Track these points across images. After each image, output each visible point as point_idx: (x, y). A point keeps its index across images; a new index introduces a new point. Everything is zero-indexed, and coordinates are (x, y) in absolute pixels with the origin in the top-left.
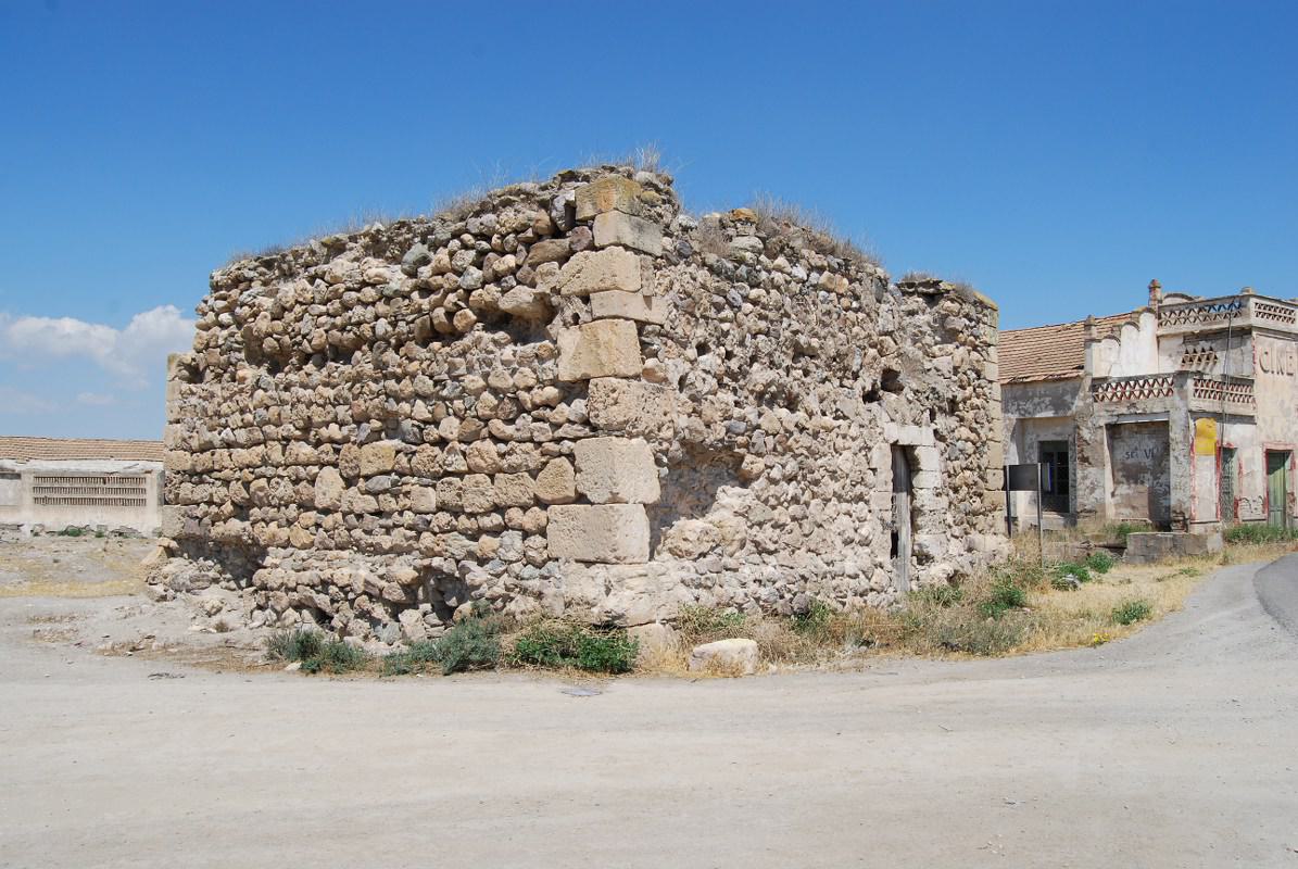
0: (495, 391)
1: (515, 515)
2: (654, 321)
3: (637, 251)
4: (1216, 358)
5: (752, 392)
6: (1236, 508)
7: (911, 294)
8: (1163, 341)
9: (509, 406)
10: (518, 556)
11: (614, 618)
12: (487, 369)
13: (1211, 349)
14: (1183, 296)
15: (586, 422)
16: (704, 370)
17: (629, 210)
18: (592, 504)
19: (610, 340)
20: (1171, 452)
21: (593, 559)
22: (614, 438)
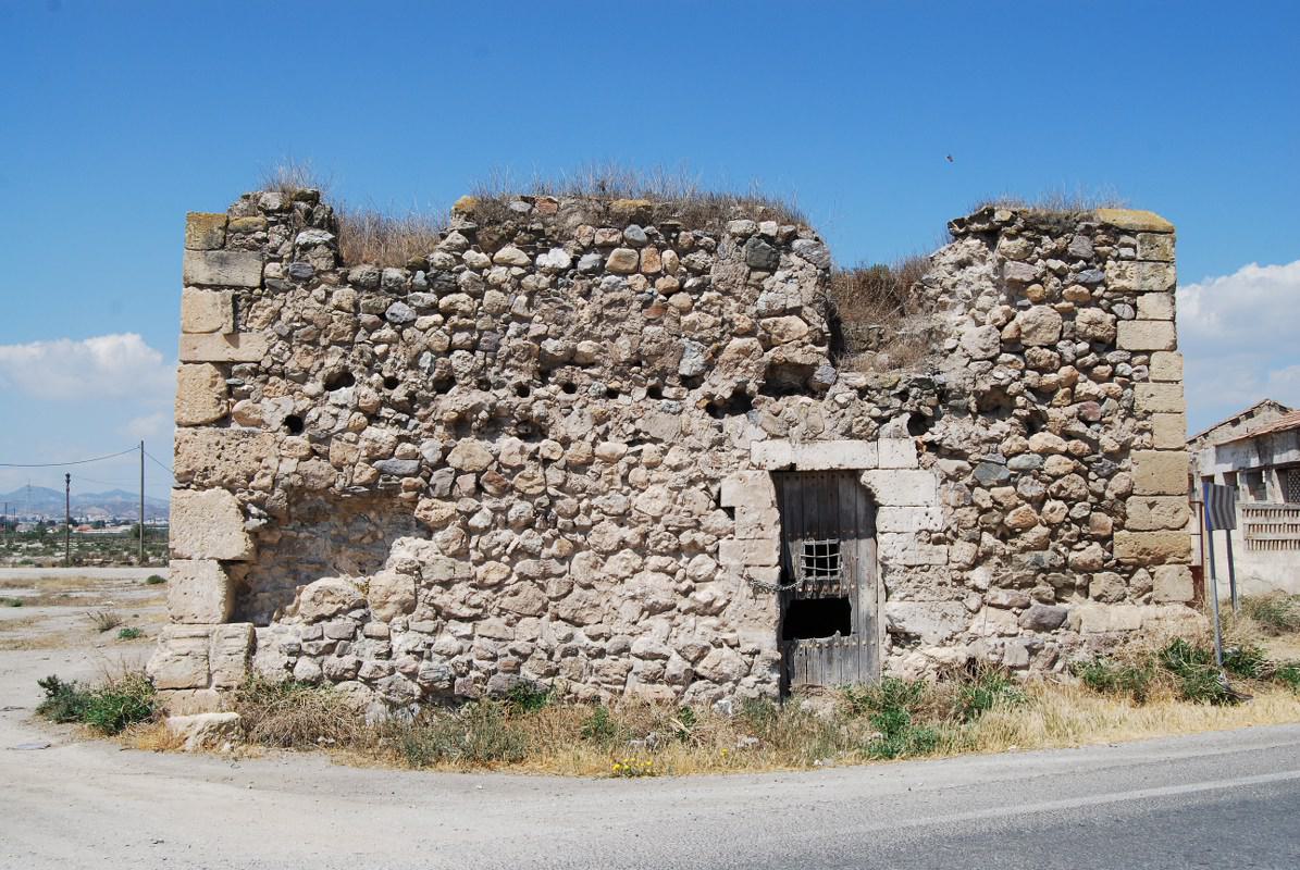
2: (244, 360)
3: (217, 287)
5: (439, 422)
7: (964, 236)
16: (336, 405)
17: (205, 246)
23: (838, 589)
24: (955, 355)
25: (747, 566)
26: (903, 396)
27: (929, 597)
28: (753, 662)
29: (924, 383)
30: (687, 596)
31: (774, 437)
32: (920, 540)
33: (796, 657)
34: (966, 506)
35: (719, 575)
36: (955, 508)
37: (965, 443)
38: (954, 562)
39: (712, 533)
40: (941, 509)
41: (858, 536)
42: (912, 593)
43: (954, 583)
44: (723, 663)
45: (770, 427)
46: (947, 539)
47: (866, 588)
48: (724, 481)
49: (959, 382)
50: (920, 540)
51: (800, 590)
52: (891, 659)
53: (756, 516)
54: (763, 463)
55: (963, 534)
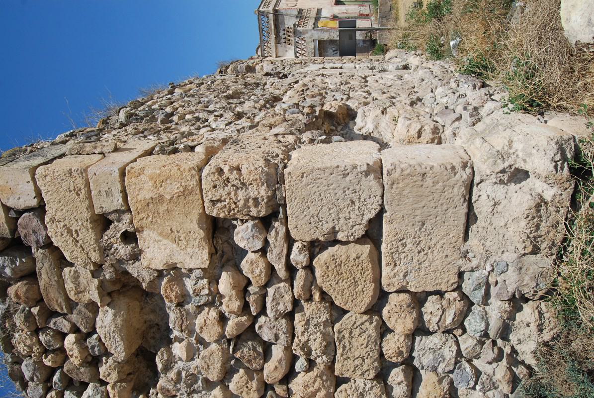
0: (228, 374)
1: (392, 345)
4: (288, 28)
6: (364, 15)
8: (279, 55)
9: (245, 350)
10: (451, 342)
11: (564, 158)
12: (200, 382)
13: (284, 30)
14: (258, 48)
15: (266, 223)
18: (382, 211)
19: (151, 178)
20: (335, 39)
21: (465, 209)
22: (286, 171)
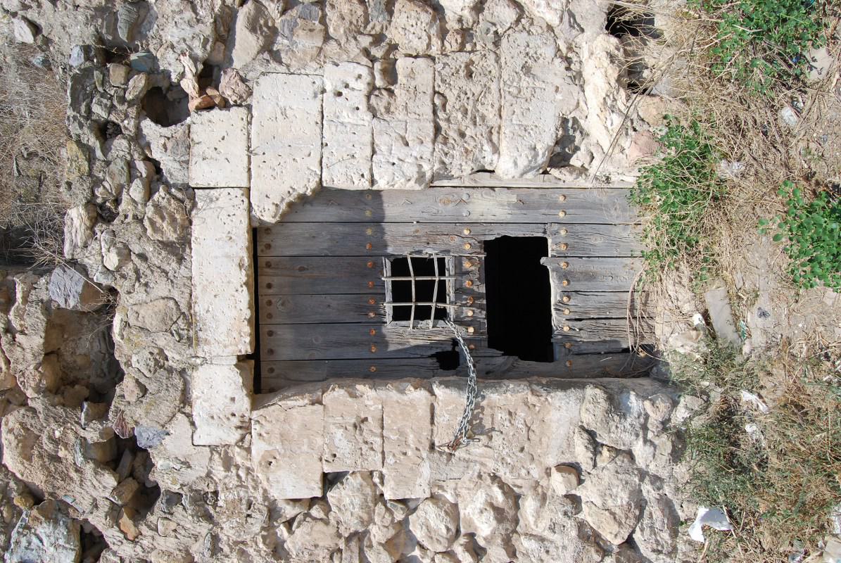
23: (470, 259)
24: (41, 22)
25: (432, 447)
26: (106, 131)
27: (492, 97)
28: (611, 449)
29: (82, 89)
30: (484, 550)
31: (185, 399)
32: (388, 110)
33: (584, 337)
34: (324, 16)
35: (449, 497)
36: (327, 38)
37: (201, 12)
38: (429, 46)
39: (370, 513)
40: (329, 67)
41: (378, 221)
42: (484, 130)
43: (468, 47)
44: (610, 503)
45: (166, 408)
46: (386, 56)
47: (470, 207)
48: (274, 493)
49: (81, 18)
50: (388, 110)
51: (471, 330)
52: (593, 170)
53: (339, 433)
54: (236, 421)
55: (377, 24)
